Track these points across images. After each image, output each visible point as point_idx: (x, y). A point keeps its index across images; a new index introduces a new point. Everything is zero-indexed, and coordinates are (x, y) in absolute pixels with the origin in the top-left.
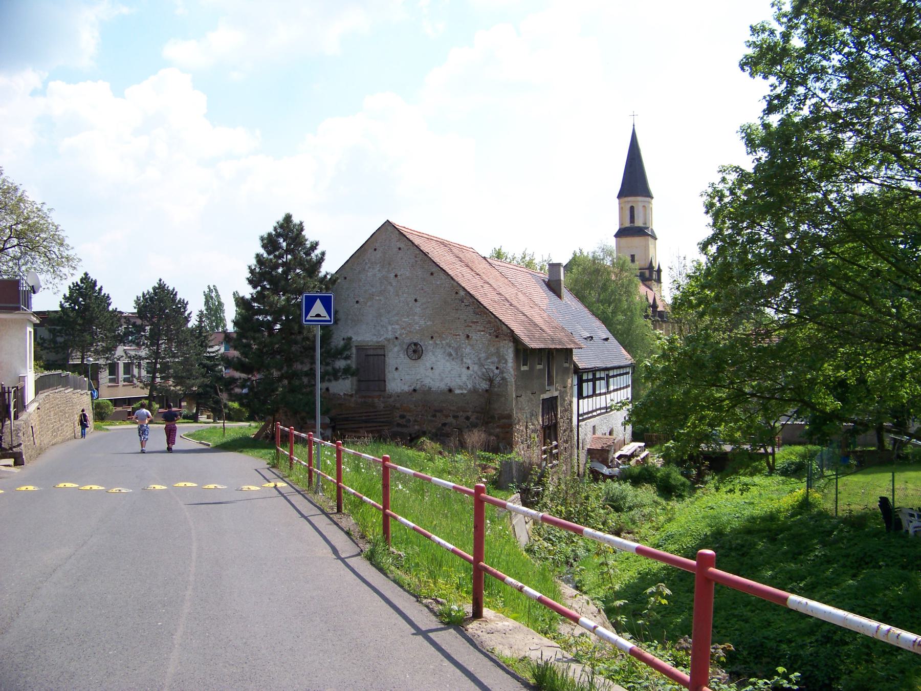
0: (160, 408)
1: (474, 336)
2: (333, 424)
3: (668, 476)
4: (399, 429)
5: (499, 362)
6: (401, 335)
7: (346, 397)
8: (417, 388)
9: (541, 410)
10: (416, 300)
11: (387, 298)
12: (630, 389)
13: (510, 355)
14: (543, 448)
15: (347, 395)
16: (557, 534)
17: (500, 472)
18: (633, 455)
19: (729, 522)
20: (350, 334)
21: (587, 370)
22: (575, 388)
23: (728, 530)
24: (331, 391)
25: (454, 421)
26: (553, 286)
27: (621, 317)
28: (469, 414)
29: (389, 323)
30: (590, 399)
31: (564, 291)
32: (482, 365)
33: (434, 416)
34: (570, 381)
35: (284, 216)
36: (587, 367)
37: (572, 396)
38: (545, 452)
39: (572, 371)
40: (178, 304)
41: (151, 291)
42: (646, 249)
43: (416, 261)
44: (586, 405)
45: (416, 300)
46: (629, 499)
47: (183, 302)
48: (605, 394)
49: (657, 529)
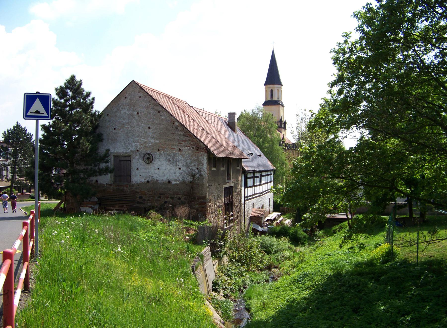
0: (19, 193)
1: (184, 149)
2: (100, 202)
3: (296, 232)
4: (139, 205)
5: (199, 165)
6: (140, 148)
7: (108, 186)
8: (150, 180)
9: (223, 194)
10: (149, 128)
11: (132, 126)
12: (272, 183)
13: (205, 160)
14: (225, 216)
15: (108, 184)
16: (233, 271)
17: (197, 233)
18: (275, 220)
19: (344, 266)
21: (250, 172)
22: (243, 182)
23: (344, 271)
24: (99, 182)
25: (171, 200)
26: (231, 125)
27: (267, 145)
28: (180, 196)
29: (133, 142)
30: (251, 188)
31: (237, 129)
32: (188, 167)
33: (160, 197)
34: (240, 178)
35: (70, 76)
36: (250, 170)
37: (241, 186)
38: (225, 219)
39: (241, 172)
40: (27, 136)
41: (12, 128)
42: (279, 112)
43: (150, 104)
44: (249, 192)
46: (275, 246)
47: (30, 135)
48: (259, 185)
49: (294, 267)
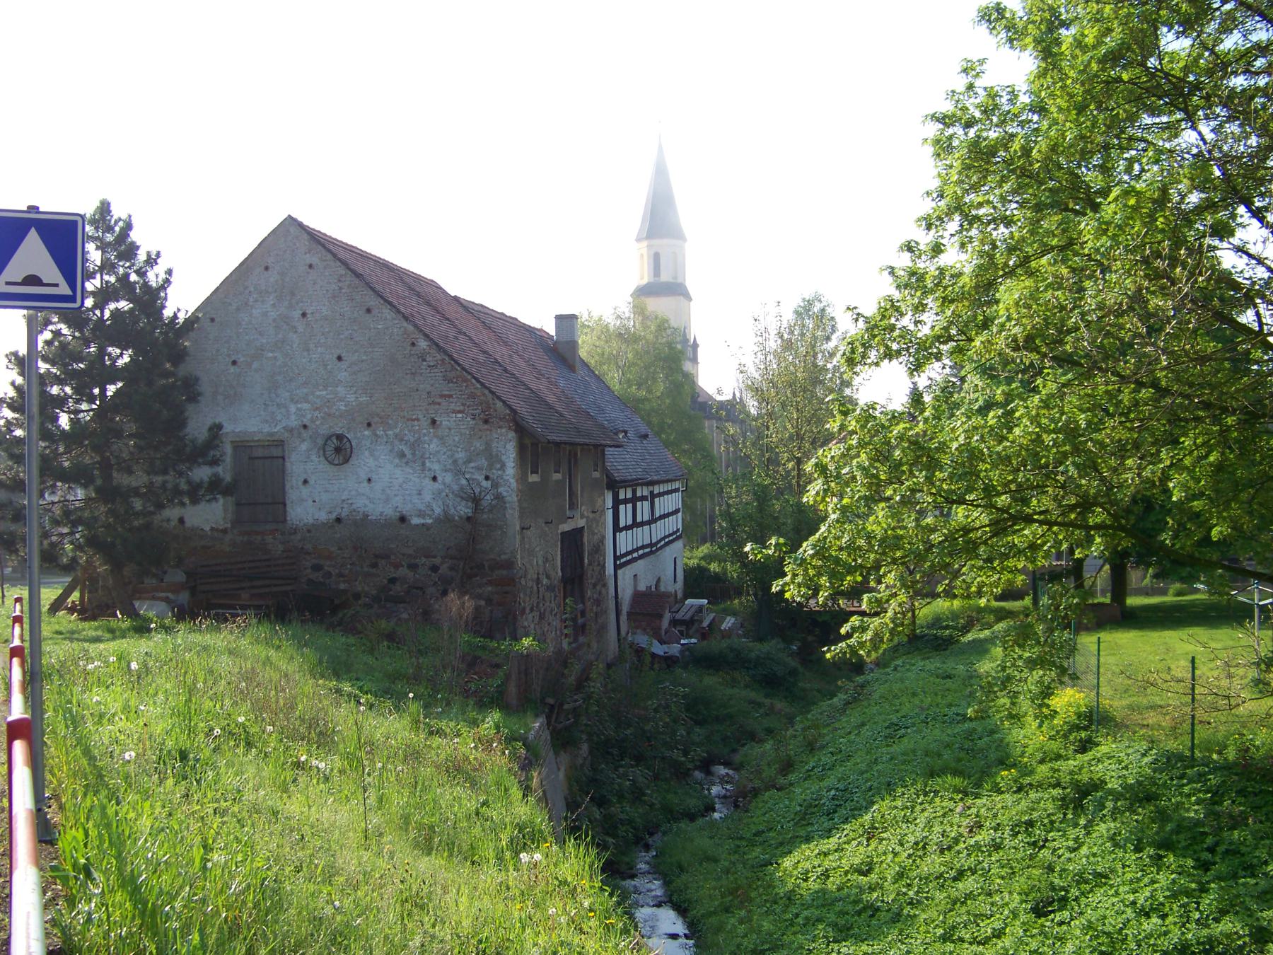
1: (445, 421)
5: (491, 467)
6: (313, 421)
7: (216, 534)
8: (343, 515)
9: (559, 553)
10: (339, 358)
15: (217, 530)
20: (222, 418)
24: (188, 524)
25: (410, 574)
28: (437, 561)
29: (292, 400)
33: (374, 565)
45: (339, 358)
